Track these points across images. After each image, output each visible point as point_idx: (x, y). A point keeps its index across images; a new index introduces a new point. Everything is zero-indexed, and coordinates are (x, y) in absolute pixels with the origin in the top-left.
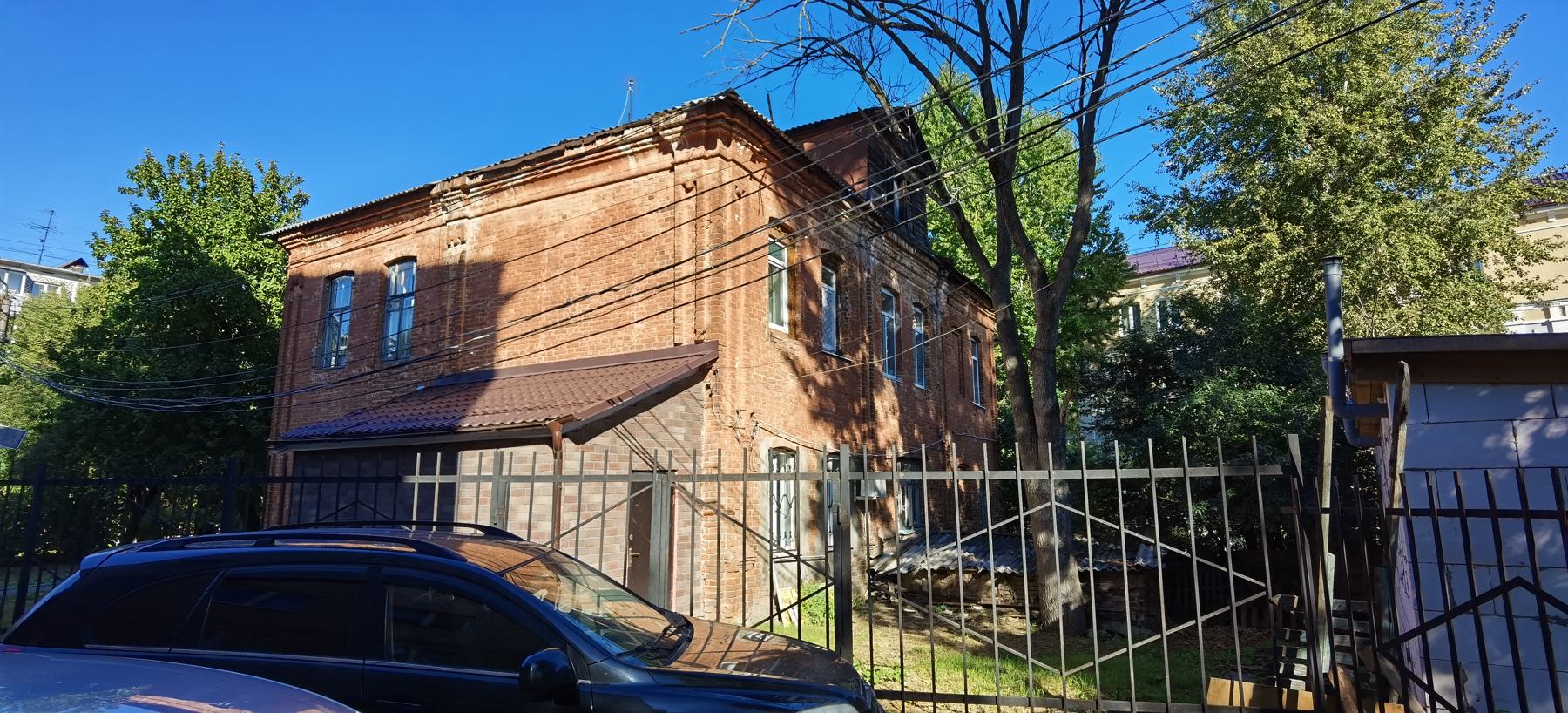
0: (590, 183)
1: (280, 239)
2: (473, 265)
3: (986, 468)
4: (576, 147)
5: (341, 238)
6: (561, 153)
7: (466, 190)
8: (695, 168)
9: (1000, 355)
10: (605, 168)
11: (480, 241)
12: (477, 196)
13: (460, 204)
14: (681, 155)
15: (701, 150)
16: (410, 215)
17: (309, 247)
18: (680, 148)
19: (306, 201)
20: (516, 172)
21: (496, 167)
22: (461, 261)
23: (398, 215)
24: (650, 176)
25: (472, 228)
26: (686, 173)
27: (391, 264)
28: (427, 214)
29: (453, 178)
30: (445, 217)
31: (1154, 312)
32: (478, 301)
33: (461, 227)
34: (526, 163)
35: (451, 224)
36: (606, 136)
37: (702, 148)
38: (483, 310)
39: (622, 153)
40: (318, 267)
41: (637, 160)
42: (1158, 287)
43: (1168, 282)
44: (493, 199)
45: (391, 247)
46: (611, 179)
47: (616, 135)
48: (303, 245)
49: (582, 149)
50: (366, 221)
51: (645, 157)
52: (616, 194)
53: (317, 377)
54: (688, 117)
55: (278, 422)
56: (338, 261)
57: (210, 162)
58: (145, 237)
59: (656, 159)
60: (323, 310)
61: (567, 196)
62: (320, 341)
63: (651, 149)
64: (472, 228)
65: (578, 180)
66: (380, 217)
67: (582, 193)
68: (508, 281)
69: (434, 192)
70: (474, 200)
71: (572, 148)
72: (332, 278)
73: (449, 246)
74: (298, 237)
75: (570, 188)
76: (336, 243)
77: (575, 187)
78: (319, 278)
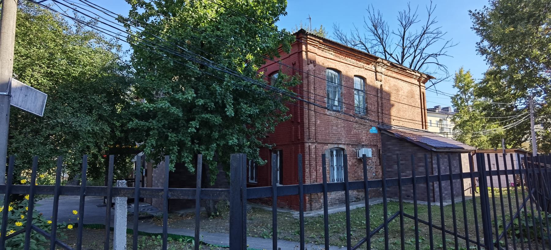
23: (361, 59)
27: (355, 76)
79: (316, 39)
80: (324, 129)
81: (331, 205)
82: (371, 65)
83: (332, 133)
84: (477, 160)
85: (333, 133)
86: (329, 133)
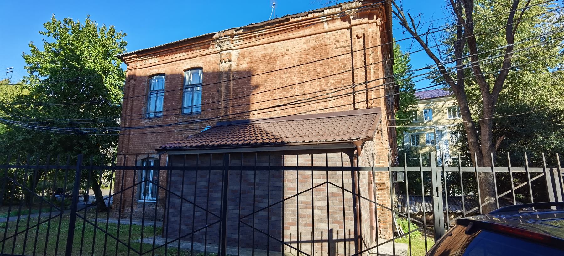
0: (301, 35)
1: (124, 58)
2: (236, 72)
3: (510, 166)
4: (297, 17)
5: (157, 58)
6: (289, 20)
7: (232, 36)
8: (363, 28)
9: (462, 121)
10: (310, 28)
11: (239, 61)
12: (238, 40)
13: (227, 43)
14: (353, 22)
15: (366, 20)
16: (199, 48)
17: (139, 62)
18: (354, 19)
19: (126, 45)
20: (262, 29)
21: (248, 27)
22: (230, 70)
23: (192, 48)
24: (336, 31)
25: (235, 54)
26: (358, 31)
27: (185, 71)
28: (208, 47)
29: (225, 31)
30: (218, 49)
31: (422, 114)
32: (240, 88)
33: (230, 54)
34: (268, 24)
35: (223, 52)
36: (314, 12)
37: (367, 19)
38: (243, 92)
39: (322, 21)
40: (144, 71)
41: (328, 24)
42: (425, 104)
43: (428, 103)
44: (247, 41)
45: (187, 63)
46: (314, 32)
47: (319, 12)
48: (136, 61)
49: (300, 18)
50: (173, 50)
51: (333, 23)
52: (317, 40)
53: (143, 122)
54: (362, 4)
55: (123, 142)
56: (156, 68)
57: (83, 24)
58: (57, 54)
59: (339, 24)
60: (147, 91)
61: (289, 41)
62: (146, 105)
63: (337, 19)
64: (235, 54)
65: (294, 33)
66: (181, 48)
67: (290, 40)
68: (255, 80)
69: (215, 37)
70: (236, 41)
71: (294, 18)
72: (151, 77)
73: (222, 62)
74: (134, 57)
75: (291, 37)
76: (155, 60)
77: (293, 36)
78: (145, 76)
79: (130, 56)
80: (136, 140)
81: (135, 218)
82: (211, 47)
83: (145, 143)
84: (551, 177)
85: (147, 143)
86: (142, 143)
